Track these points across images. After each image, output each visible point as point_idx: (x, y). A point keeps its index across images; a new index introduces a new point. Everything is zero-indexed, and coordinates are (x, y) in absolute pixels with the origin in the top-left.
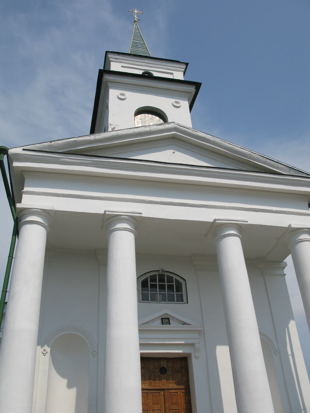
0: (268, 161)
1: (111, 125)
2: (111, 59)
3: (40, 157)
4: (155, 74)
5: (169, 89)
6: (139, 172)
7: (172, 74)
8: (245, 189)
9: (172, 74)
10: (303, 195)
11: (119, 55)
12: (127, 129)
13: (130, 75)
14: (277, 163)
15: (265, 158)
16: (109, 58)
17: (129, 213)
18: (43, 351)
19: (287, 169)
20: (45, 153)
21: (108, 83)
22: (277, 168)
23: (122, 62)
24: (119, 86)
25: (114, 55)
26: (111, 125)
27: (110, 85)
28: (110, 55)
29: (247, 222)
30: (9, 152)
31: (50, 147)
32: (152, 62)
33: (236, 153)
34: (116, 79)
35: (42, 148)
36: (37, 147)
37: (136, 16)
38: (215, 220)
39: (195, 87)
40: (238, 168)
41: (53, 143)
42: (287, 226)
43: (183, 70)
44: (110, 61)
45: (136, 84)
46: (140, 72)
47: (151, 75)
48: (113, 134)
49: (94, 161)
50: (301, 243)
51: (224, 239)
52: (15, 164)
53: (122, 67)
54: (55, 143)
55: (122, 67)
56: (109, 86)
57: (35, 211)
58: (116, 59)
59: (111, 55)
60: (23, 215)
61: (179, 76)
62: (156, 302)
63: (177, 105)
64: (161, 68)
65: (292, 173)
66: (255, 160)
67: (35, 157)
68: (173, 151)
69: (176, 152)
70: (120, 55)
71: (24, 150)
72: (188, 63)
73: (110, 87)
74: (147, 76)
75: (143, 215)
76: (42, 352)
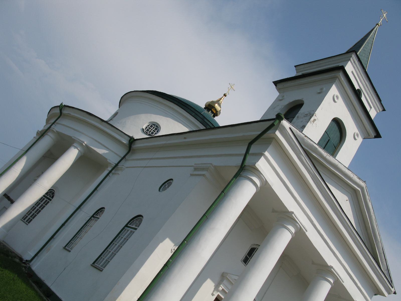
0: (383, 254)
1: (315, 116)
2: (351, 59)
3: (296, 148)
4: (363, 99)
5: (361, 121)
6: (327, 203)
7: (371, 108)
8: (358, 260)
9: (371, 108)
10: (376, 286)
11: (358, 61)
12: (344, 166)
13: (353, 88)
14: (385, 260)
15: (383, 252)
16: (351, 57)
17: (302, 225)
18: (173, 249)
19: (386, 268)
20: (300, 146)
21: (337, 79)
22: (382, 262)
23: (355, 68)
24: (341, 89)
25: (356, 59)
26: (315, 116)
27: (337, 81)
28: (354, 55)
29: (307, 231)
30: (282, 122)
31: (303, 139)
32: (371, 91)
33: (373, 234)
34: (344, 82)
35: (298, 136)
36: (297, 132)
37: (381, 20)
38: (293, 213)
39: (375, 135)
40: (364, 240)
41: (306, 138)
42: (290, 211)
43: (378, 111)
44: (350, 60)
45: (343, 85)
46: (357, 87)
47: (360, 94)
48: (336, 163)
49: (316, 175)
50: (287, 231)
51: (248, 181)
52: (278, 133)
53: (352, 72)
54: (307, 140)
55: (352, 72)
56: (335, 81)
57: (262, 178)
58: (354, 62)
59: (354, 56)
60: (252, 171)
61: (373, 113)
62: (245, 264)
63: (356, 137)
64: (369, 96)
65: (386, 272)
66: (377, 247)
67: (291, 140)
68: (348, 199)
69: (348, 201)
70: (359, 62)
71: (290, 128)
72: (386, 111)
73: (335, 82)
74: (358, 94)
75: (307, 233)
76: (172, 250)
